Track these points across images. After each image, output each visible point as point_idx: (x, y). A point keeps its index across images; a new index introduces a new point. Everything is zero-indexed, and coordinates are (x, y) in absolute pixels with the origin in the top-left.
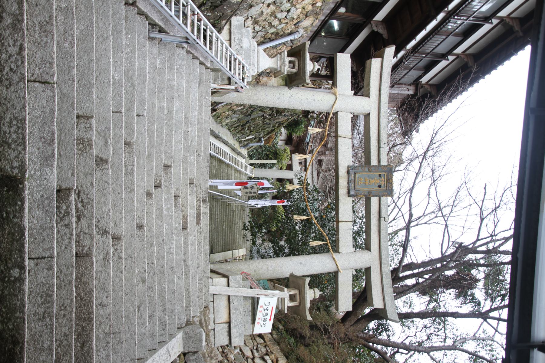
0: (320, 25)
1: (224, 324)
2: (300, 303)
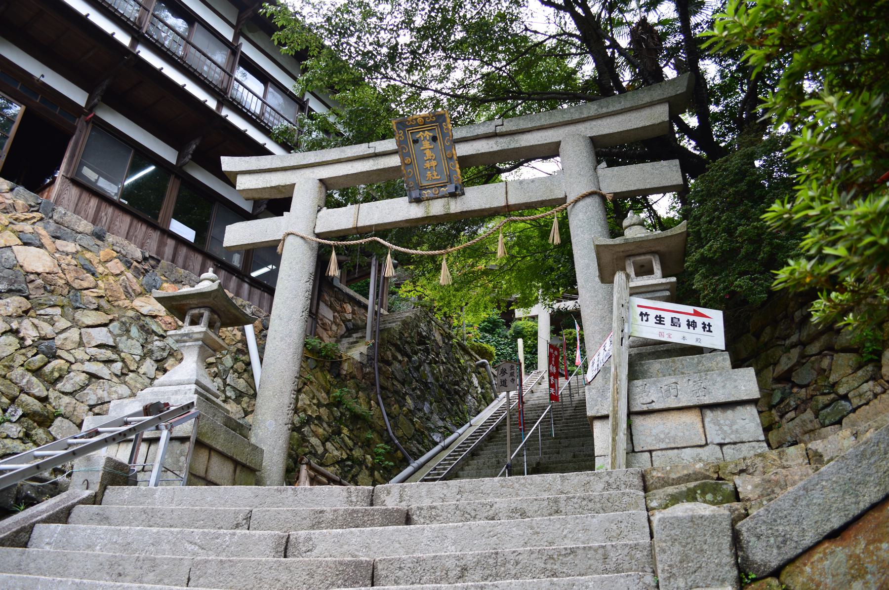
0: (260, 289)
1: (707, 420)
2: (653, 253)
